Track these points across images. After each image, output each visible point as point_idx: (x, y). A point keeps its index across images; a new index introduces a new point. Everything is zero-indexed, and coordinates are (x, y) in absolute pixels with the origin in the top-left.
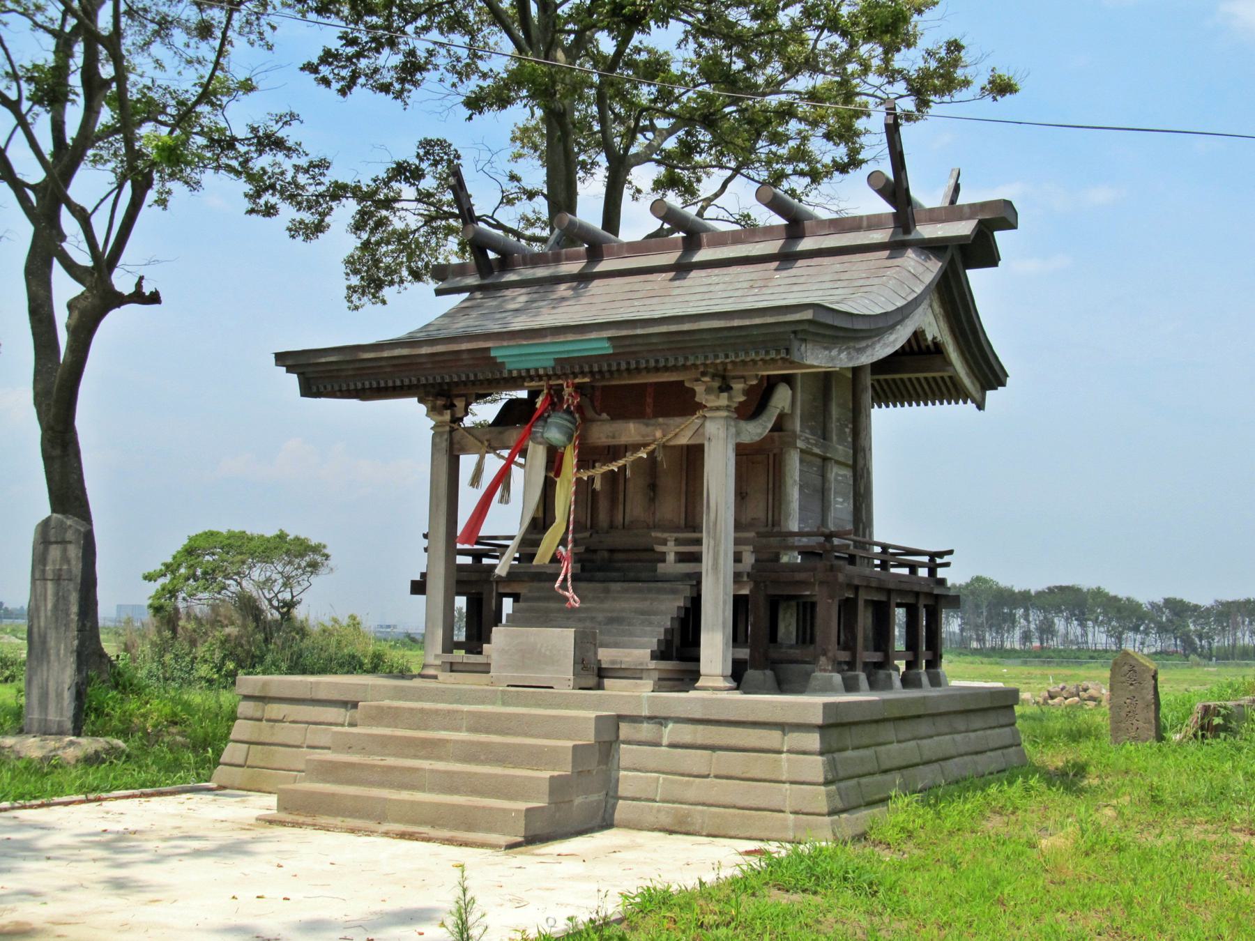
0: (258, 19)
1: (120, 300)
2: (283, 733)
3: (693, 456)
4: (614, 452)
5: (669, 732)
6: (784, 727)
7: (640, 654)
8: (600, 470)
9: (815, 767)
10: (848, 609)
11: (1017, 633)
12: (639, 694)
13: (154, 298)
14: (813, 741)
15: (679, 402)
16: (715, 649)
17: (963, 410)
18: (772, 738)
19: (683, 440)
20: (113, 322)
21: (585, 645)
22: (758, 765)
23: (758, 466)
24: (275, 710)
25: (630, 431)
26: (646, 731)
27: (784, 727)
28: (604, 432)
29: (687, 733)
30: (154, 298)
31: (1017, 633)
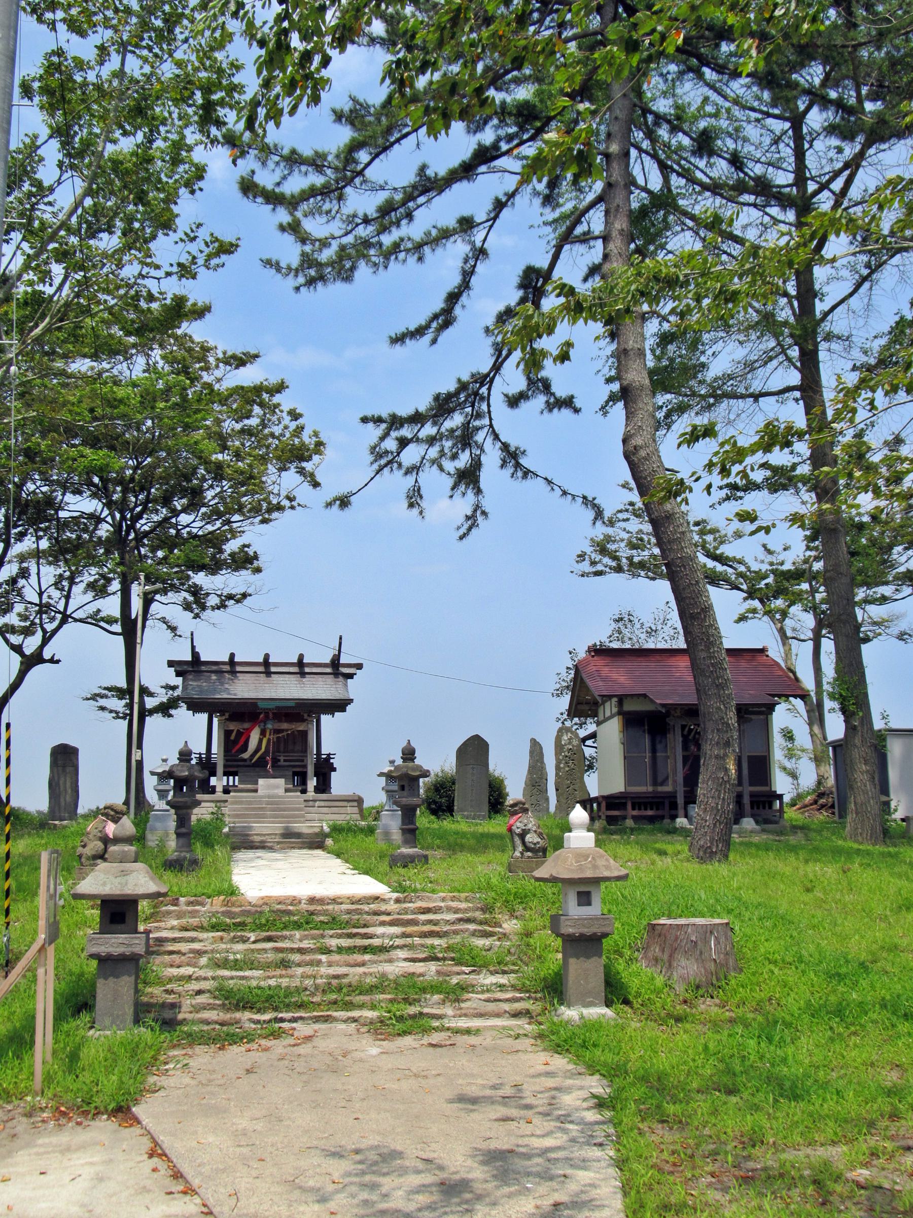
1: (44, 661)
5: (317, 804)
13: (58, 662)
18: (345, 804)
19: (301, 729)
22: (342, 810)
25: (285, 726)
29: (322, 804)
30: (58, 662)
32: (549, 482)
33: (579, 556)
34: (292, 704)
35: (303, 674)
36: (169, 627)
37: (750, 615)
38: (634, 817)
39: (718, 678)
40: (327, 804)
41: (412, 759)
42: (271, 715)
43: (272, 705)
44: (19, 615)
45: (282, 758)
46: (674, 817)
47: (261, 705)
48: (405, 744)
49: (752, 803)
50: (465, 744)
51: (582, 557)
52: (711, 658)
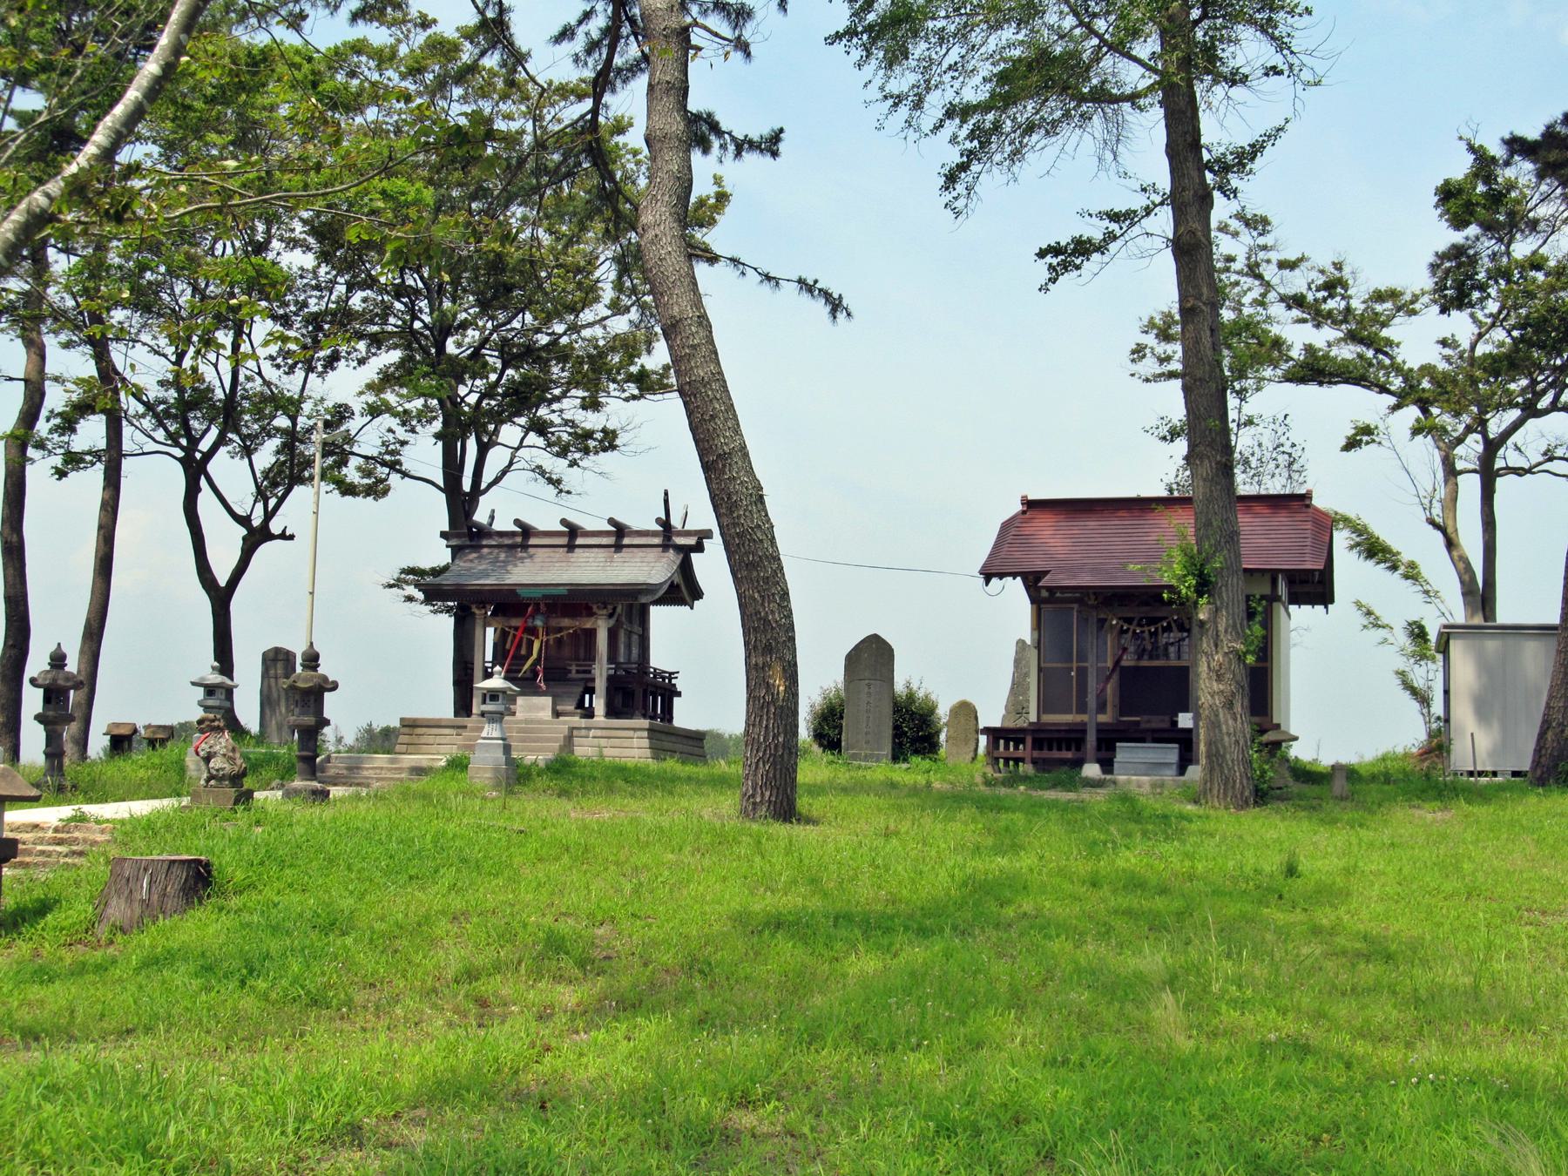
0: (1365, 1096)
1: (272, 537)
2: (423, 740)
3: (591, 634)
4: (560, 630)
5: (592, 733)
6: (634, 729)
7: (571, 708)
8: (552, 637)
9: (646, 743)
10: (645, 692)
11: (644, 816)
12: (576, 720)
13: (291, 537)
14: (645, 734)
15: (590, 614)
16: (599, 705)
17: (683, 610)
18: (631, 733)
19: (588, 626)
20: (265, 551)
21: (554, 704)
22: (626, 743)
23: (613, 635)
24: (419, 731)
25: (566, 622)
26: (583, 732)
27: (634, 729)
28: (554, 622)
29: (599, 733)
30: (291, 537)
31: (644, 816)
32: (735, 261)
33: (1133, 352)
34: (562, 591)
35: (618, 547)
36: (550, 481)
37: (1365, 438)
38: (1034, 762)
39: (747, 553)
40: (605, 733)
41: (315, 668)
42: (542, 607)
43: (537, 593)
44: (359, 469)
45: (574, 668)
46: (1078, 763)
47: (523, 593)
48: (54, 647)
49: (1099, 740)
50: (858, 649)
51: (1139, 352)
52: (735, 525)
